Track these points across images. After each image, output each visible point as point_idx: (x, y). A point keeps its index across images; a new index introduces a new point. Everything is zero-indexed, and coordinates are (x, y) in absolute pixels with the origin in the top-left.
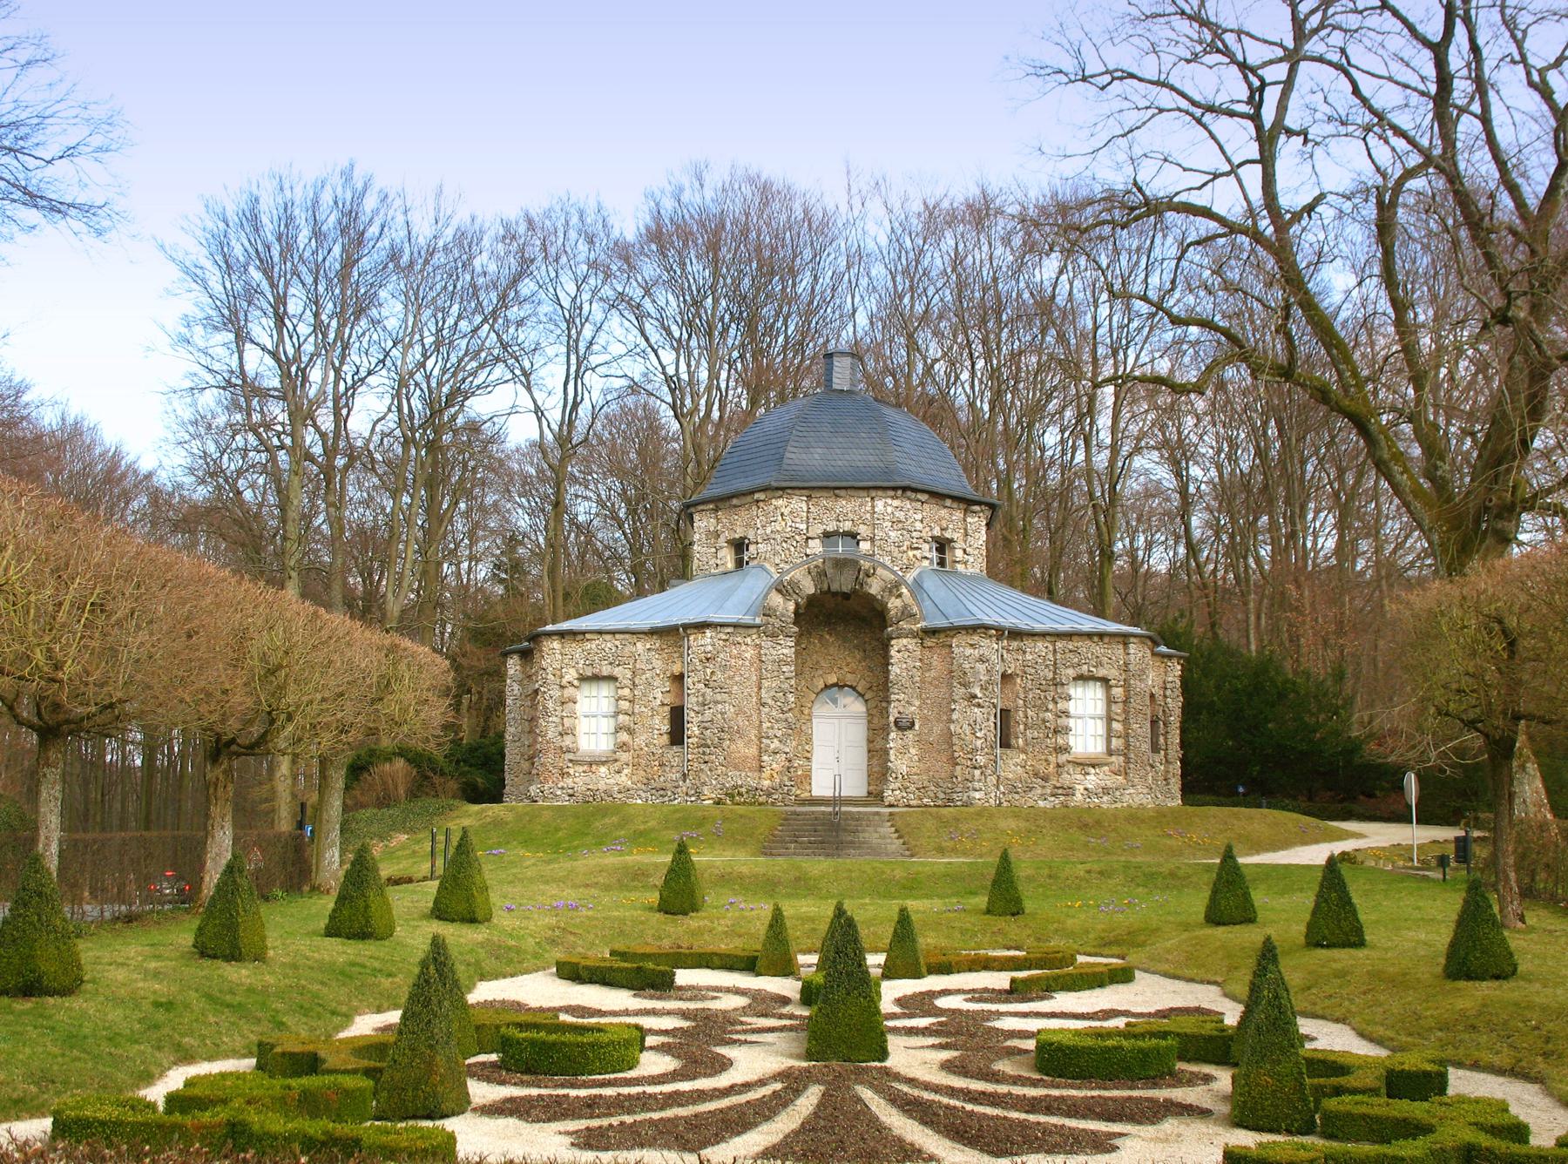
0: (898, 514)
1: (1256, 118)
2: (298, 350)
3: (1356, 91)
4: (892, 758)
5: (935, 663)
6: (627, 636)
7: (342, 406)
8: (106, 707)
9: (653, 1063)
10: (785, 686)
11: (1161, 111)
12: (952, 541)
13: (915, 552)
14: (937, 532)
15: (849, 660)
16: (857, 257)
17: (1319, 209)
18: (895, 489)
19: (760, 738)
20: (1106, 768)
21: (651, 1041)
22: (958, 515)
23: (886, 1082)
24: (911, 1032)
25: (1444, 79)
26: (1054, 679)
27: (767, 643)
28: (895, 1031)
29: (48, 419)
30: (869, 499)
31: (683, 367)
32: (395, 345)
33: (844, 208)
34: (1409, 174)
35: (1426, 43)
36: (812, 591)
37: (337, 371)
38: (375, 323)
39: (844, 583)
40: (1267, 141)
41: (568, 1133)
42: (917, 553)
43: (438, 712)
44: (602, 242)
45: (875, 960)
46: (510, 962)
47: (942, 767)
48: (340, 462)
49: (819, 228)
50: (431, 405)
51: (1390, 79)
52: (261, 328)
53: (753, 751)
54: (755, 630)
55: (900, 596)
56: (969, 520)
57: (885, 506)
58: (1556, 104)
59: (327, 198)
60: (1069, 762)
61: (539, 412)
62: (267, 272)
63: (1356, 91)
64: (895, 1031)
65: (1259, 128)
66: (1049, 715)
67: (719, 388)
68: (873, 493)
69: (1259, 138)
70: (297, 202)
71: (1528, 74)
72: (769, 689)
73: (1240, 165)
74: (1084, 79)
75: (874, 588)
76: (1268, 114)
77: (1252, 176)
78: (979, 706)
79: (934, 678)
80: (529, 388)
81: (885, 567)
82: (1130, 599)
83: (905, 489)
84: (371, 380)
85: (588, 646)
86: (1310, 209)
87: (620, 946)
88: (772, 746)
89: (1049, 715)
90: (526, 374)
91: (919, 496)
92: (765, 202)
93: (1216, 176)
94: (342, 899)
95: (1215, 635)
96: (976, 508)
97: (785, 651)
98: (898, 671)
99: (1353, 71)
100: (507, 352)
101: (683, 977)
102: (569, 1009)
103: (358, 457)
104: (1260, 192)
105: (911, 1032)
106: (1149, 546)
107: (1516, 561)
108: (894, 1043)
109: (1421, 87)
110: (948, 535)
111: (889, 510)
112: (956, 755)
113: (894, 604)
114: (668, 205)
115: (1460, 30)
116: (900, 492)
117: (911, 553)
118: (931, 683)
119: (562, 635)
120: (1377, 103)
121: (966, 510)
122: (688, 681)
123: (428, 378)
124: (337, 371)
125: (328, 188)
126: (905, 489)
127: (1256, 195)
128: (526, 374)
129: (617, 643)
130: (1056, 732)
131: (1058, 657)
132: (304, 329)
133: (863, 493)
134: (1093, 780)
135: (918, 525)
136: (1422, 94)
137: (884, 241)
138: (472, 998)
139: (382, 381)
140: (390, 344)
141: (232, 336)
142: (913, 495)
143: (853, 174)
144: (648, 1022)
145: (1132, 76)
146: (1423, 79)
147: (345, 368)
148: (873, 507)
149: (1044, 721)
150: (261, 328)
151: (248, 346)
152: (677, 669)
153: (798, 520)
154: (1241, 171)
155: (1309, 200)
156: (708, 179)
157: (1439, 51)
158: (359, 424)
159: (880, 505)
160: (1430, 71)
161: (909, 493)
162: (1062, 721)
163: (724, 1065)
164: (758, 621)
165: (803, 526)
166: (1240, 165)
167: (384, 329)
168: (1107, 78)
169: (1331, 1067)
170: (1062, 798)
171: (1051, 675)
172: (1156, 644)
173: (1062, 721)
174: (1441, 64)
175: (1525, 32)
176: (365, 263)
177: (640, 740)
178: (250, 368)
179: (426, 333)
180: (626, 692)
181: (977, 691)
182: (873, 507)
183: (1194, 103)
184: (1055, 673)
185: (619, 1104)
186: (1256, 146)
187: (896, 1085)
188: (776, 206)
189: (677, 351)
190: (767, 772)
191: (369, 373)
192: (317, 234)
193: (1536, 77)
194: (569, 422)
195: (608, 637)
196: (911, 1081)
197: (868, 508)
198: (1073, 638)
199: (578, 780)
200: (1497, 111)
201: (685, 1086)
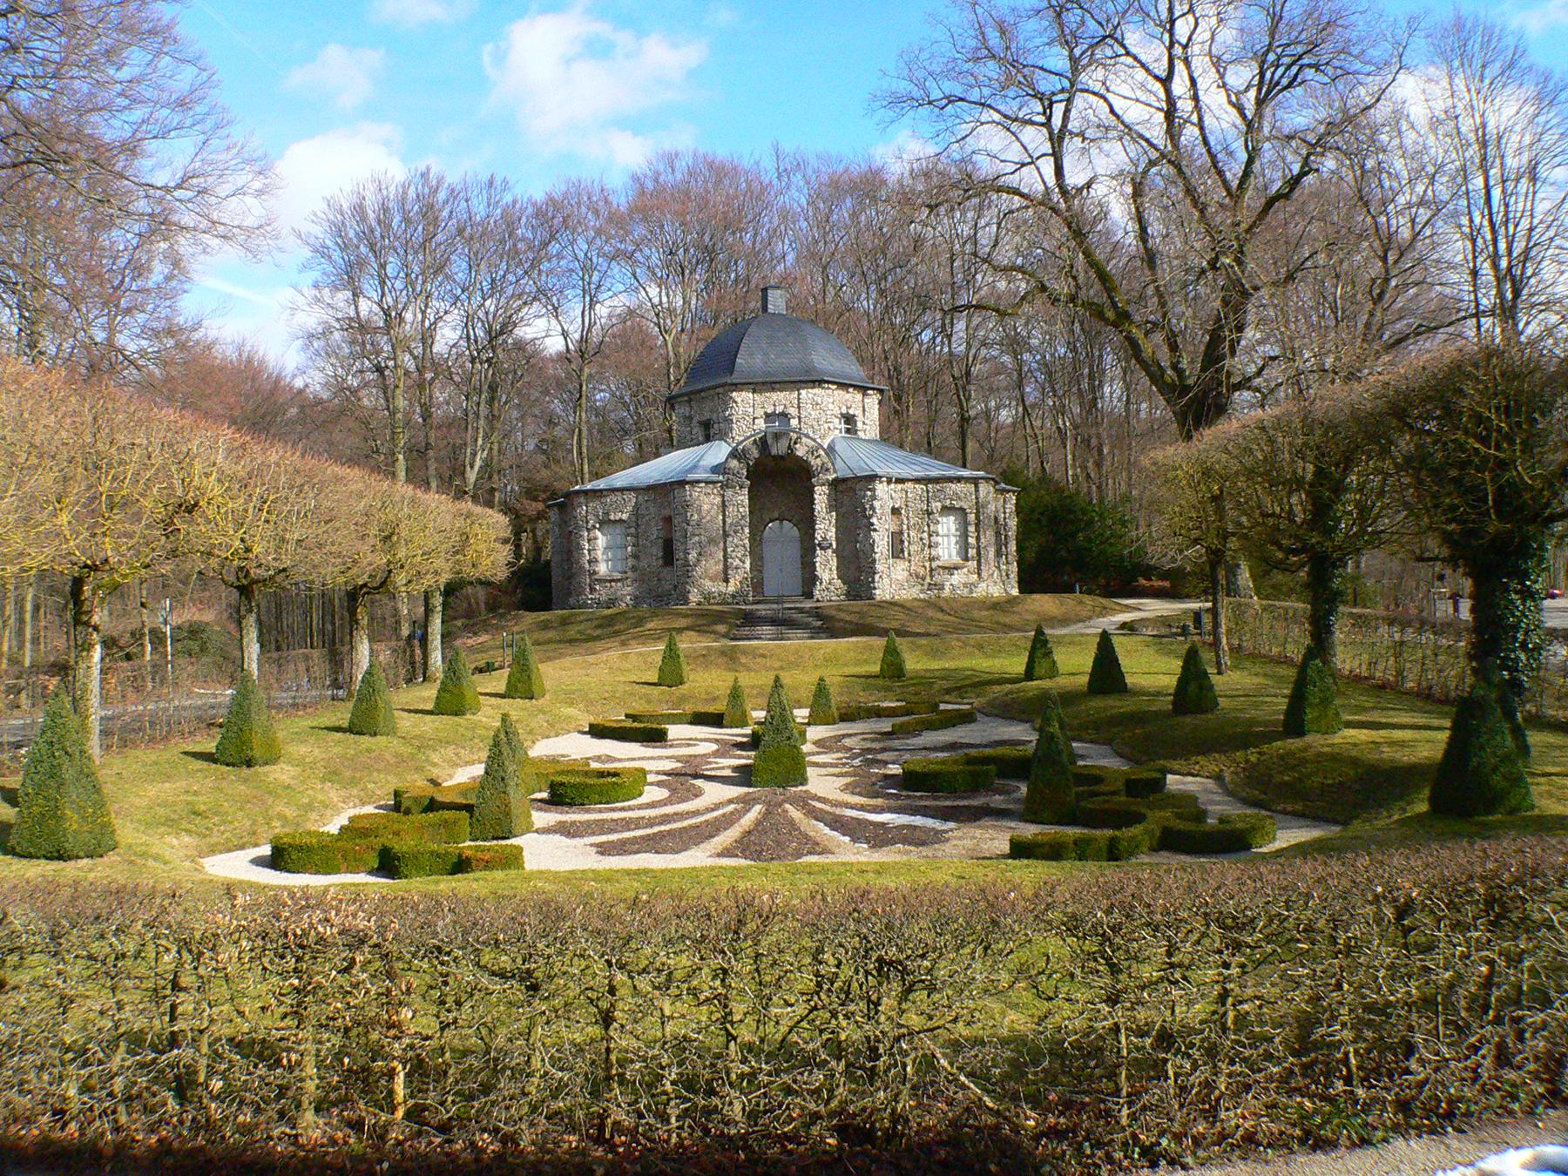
1: (1047, 124)
2: (396, 301)
3: (1112, 111)
7: (427, 337)
8: (280, 571)
9: (652, 794)
11: (982, 124)
14: (844, 410)
16: (785, 215)
17: (1094, 186)
21: (651, 778)
22: (859, 396)
23: (803, 802)
24: (824, 765)
25: (1171, 101)
28: (817, 765)
29: (226, 351)
31: (665, 299)
32: (463, 291)
33: (775, 181)
34: (1152, 163)
35: (1157, 78)
37: (423, 313)
38: (447, 277)
40: (1057, 140)
41: (591, 845)
43: (504, 553)
44: (604, 212)
45: (801, 714)
46: (555, 728)
48: (429, 376)
49: (758, 194)
50: (489, 332)
51: (1137, 100)
52: (370, 287)
58: (673, 723)
59: (412, 193)
61: (565, 334)
62: (372, 247)
63: (1112, 111)
64: (817, 765)
65: (1051, 133)
67: (690, 311)
69: (1051, 139)
70: (392, 197)
71: (1229, 96)
72: (731, 524)
73: (1038, 158)
74: (930, 103)
75: (801, 451)
76: (1057, 122)
77: (1047, 167)
80: (557, 317)
81: (807, 436)
82: (986, 444)
84: (448, 318)
86: (1089, 185)
87: (628, 712)
90: (556, 309)
92: (718, 182)
93: (1023, 165)
94: (443, 689)
95: (1043, 469)
96: (870, 392)
99: (1109, 96)
100: (541, 294)
101: (674, 731)
102: (598, 758)
103: (439, 367)
104: (1054, 178)
105: (824, 765)
106: (998, 408)
108: (811, 772)
109: (1157, 104)
114: (650, 185)
115: (1180, 67)
117: (826, 426)
119: (586, 492)
120: (1128, 118)
122: (675, 522)
123: (487, 313)
124: (423, 313)
125: (412, 189)
127: (1051, 180)
128: (556, 309)
130: (930, 547)
132: (399, 285)
134: (957, 578)
135: (831, 406)
136: (1158, 109)
137: (803, 201)
138: (533, 753)
139: (455, 316)
140: (459, 291)
141: (349, 294)
143: (781, 157)
144: (647, 765)
145: (961, 99)
146: (1159, 100)
147: (429, 311)
150: (370, 287)
151: (361, 299)
152: (667, 512)
154: (1039, 162)
155: (1087, 179)
156: (677, 165)
157: (1166, 82)
158: (440, 347)
159: (803, 392)
160: (1162, 95)
163: (698, 793)
165: (751, 410)
166: (1038, 158)
167: (454, 281)
168: (944, 102)
169: (1093, 779)
172: (997, 483)
174: (1168, 92)
175: (1225, 69)
176: (440, 237)
177: (644, 564)
178: (364, 313)
179: (484, 283)
180: (633, 530)
183: (1006, 116)
185: (627, 824)
186: (1049, 144)
187: (813, 803)
188: (727, 182)
189: (660, 286)
190: (732, 581)
191: (446, 313)
192: (406, 220)
193: (1234, 99)
194: (584, 340)
196: (820, 799)
199: (602, 592)
200: (1208, 120)
201: (668, 810)
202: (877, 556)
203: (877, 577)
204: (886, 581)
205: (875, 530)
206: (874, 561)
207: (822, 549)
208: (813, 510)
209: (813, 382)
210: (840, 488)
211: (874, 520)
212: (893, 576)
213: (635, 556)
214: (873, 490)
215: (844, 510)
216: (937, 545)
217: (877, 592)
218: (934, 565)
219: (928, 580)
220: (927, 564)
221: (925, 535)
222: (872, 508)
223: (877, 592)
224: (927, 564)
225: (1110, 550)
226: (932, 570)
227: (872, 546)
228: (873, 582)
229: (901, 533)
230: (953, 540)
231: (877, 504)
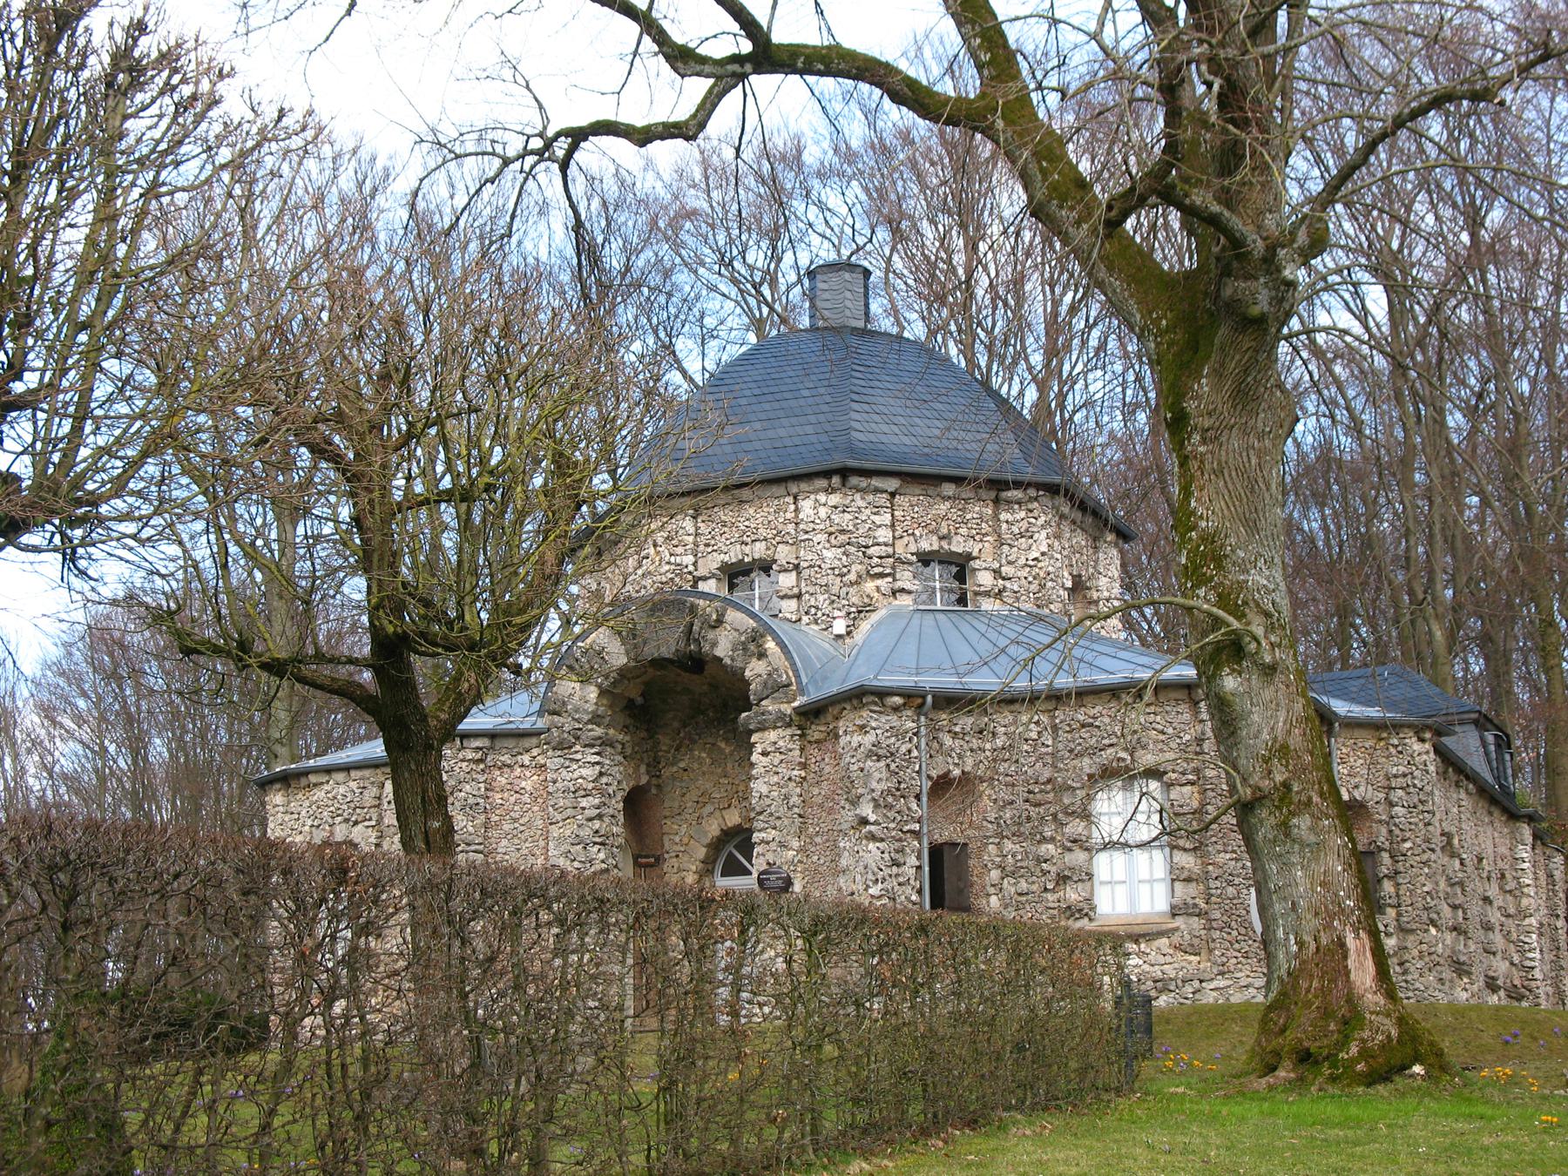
0: (845, 520)
5: (827, 769)
6: (367, 773)
10: (586, 833)
12: (969, 557)
13: (879, 582)
18: (827, 474)
20: (1164, 941)
27: (553, 761)
30: (790, 499)
36: (623, 660)
39: (666, 643)
54: (534, 741)
55: (762, 655)
56: (1004, 516)
57: (816, 506)
66: (1049, 849)
68: (794, 489)
72: (560, 840)
75: (723, 646)
78: (872, 837)
83: (845, 473)
85: (319, 794)
89: (1049, 849)
91: (876, 482)
97: (584, 772)
98: (764, 790)
110: (958, 546)
111: (823, 512)
113: (755, 670)
116: (836, 480)
118: (821, 806)
121: (996, 501)
126: (845, 473)
129: (353, 785)
130: (1062, 879)
133: (780, 490)
142: (863, 483)
148: (797, 510)
149: (1040, 860)
153: (680, 550)
161: (854, 480)
164: (541, 724)
181: (867, 810)
182: (797, 510)
195: (340, 776)
197: (789, 515)
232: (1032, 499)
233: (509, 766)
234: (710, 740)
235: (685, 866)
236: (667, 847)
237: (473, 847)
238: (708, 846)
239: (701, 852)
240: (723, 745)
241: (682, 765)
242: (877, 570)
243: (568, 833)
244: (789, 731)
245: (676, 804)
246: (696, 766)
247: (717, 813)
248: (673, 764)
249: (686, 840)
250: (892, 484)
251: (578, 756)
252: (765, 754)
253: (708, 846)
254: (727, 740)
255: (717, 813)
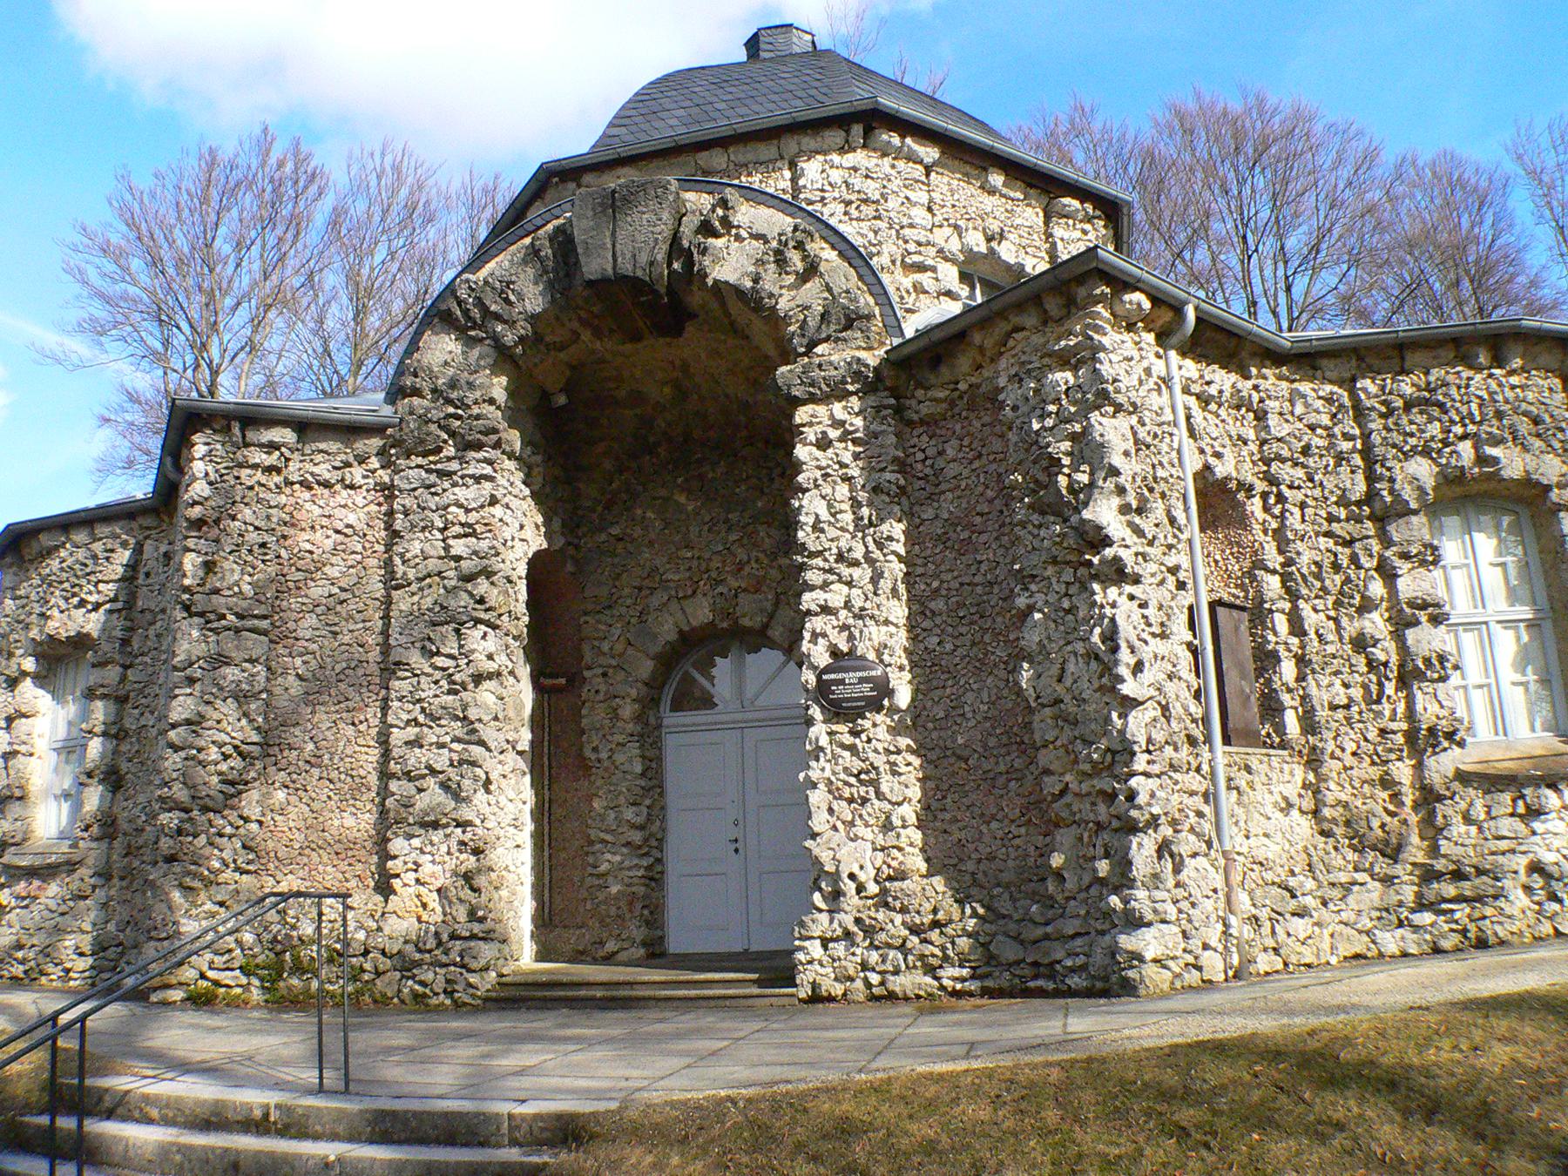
4: (819, 821)
14: (977, 241)
15: (741, 554)
19: (385, 775)
26: (1371, 496)
42: (925, 279)
47: (1007, 838)
53: (358, 822)
60: (1463, 777)
72: (412, 617)
79: (952, 523)
88: (422, 802)
96: (1072, 203)
107: (1113, 951)
111: (836, 176)
112: (1051, 785)
130: (1408, 677)
131: (1376, 424)
159: (812, 169)
162: (1424, 639)
170: (1462, 912)
171: (1359, 488)
173: (1424, 639)
184: (1371, 478)
190: (405, 890)
195: (80, 537)
198: (1412, 358)
202: (1138, 725)
203: (1142, 850)
204: (1201, 873)
205: (1118, 574)
206: (1125, 751)
207: (838, 711)
208: (790, 523)
209: (842, 121)
210: (924, 405)
211: (1104, 512)
212: (1234, 839)
213: (113, 778)
214: (1085, 357)
215: (948, 506)
216: (1442, 666)
217: (1149, 943)
218: (1442, 765)
219: (1416, 850)
220: (1403, 771)
221: (1376, 624)
222: (1088, 450)
223: (1149, 943)
224: (1403, 771)
225: (1123, 671)
226: (1429, 798)
227: (1104, 662)
228: (1122, 880)
229: (1259, 614)
230: (1507, 644)
231: (1112, 430)
232: (1089, 220)
233: (326, 485)
234: (663, 492)
235: (620, 689)
236: (588, 657)
237: (249, 623)
238: (657, 657)
239: (646, 668)
240: (682, 499)
241: (615, 531)
242: (916, 258)
243: (428, 602)
244: (872, 400)
245: (604, 591)
246: (638, 532)
247: (674, 605)
248: (602, 529)
249: (619, 647)
250: (930, 153)
251: (454, 466)
252: (823, 443)
253: (657, 657)
254: (688, 491)
255: (674, 605)
